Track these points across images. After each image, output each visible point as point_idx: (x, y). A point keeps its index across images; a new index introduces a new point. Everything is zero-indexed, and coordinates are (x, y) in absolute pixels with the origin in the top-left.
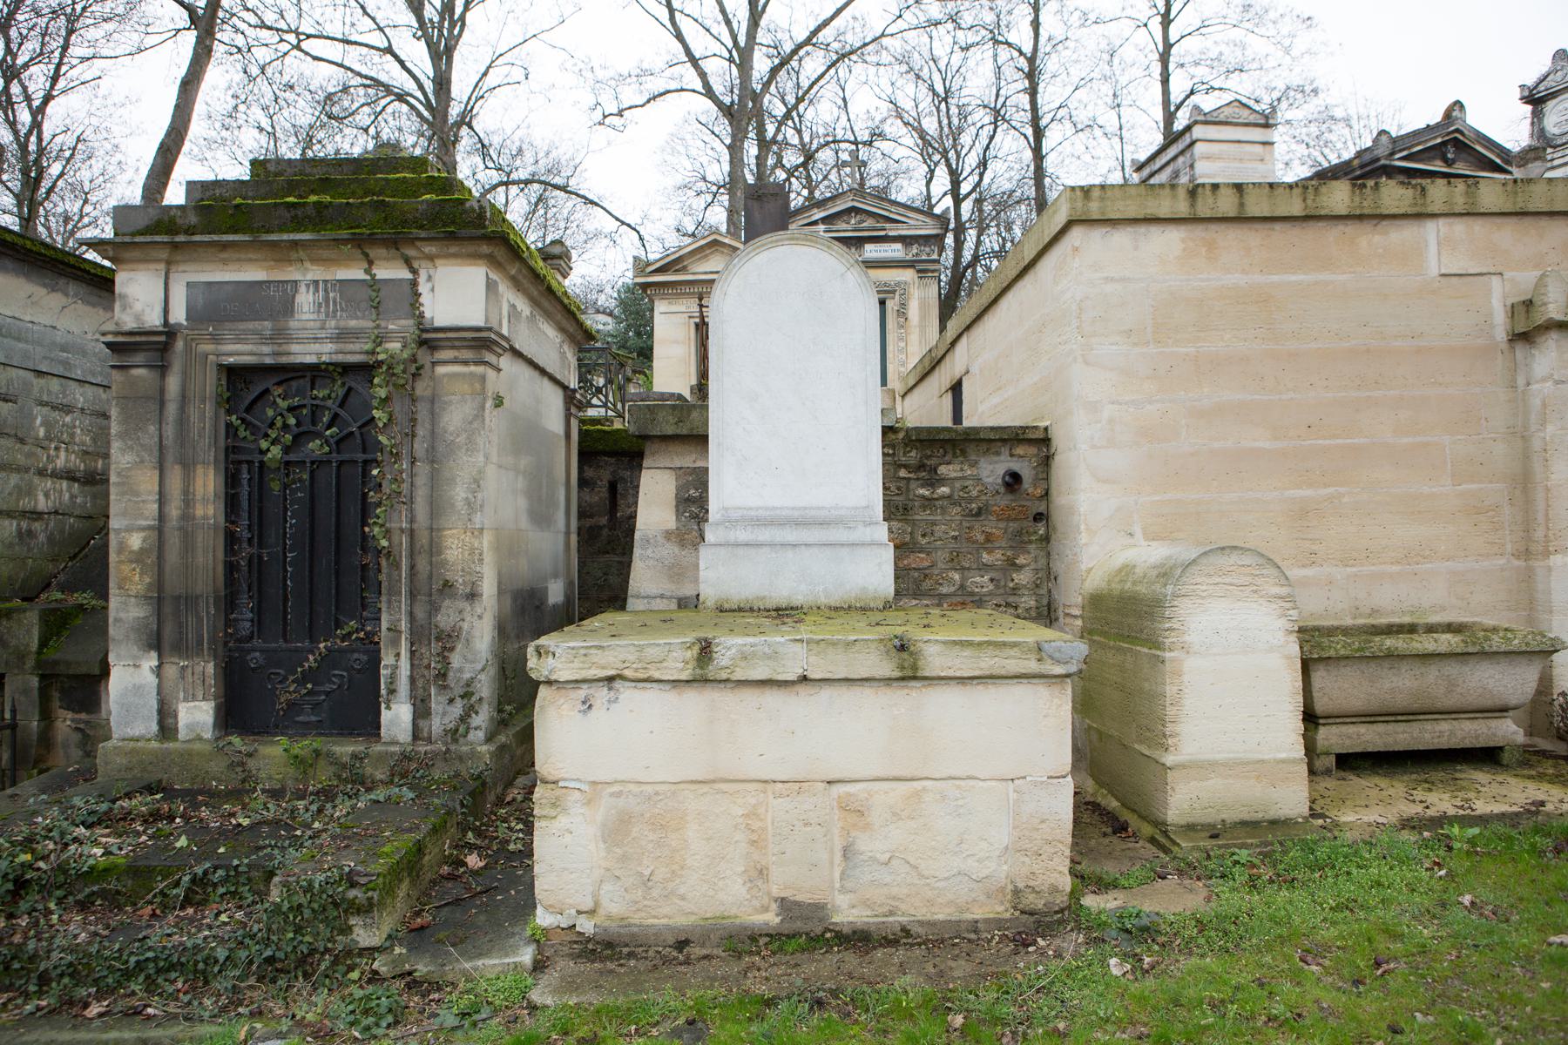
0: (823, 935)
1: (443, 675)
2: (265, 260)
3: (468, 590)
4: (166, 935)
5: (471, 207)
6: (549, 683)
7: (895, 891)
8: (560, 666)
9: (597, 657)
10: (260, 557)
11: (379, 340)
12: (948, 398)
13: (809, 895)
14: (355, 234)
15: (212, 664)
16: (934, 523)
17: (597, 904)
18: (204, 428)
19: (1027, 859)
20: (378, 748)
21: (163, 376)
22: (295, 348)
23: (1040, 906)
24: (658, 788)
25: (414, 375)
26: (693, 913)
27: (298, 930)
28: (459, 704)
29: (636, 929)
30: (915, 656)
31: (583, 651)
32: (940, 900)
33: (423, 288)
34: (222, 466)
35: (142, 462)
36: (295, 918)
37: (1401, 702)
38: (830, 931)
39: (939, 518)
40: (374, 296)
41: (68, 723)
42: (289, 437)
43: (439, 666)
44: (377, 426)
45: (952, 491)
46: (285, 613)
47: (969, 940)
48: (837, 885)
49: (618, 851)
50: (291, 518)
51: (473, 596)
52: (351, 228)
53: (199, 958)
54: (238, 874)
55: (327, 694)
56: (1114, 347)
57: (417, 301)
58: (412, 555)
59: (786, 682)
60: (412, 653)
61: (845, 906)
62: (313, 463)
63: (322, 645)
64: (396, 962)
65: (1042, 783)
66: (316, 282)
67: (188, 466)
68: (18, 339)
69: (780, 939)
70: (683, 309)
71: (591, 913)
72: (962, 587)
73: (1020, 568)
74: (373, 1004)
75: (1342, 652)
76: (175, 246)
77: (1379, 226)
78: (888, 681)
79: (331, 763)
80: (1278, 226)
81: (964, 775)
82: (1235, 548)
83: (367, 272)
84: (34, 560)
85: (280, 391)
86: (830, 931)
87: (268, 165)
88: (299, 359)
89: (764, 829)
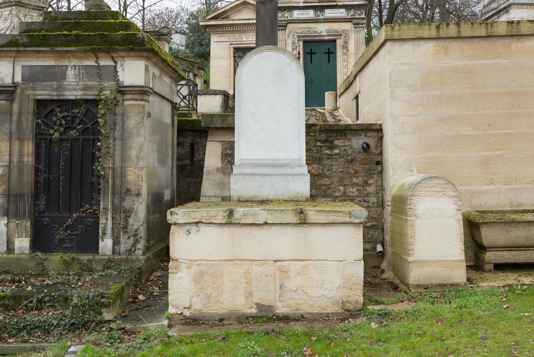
0: (272, 317)
1: (125, 227)
2: (54, 57)
3: (136, 192)
4: (32, 317)
5: (139, 37)
6: (175, 224)
7: (299, 302)
8: (179, 218)
9: (193, 215)
10: (49, 178)
11: (101, 91)
12: (355, 101)
13: (267, 302)
14: (92, 48)
15: (29, 222)
16: (332, 165)
17: (191, 305)
18: (28, 125)
20: (98, 257)
21: (12, 104)
22: (66, 93)
23: (352, 308)
24: (214, 262)
25: (115, 105)
26: (226, 309)
27: (84, 313)
29: (205, 314)
30: (305, 215)
31: (188, 213)
32: (315, 305)
33: (119, 69)
34: (34, 140)
35: (3, 139)
36: (83, 308)
37: (521, 242)
38: (275, 316)
39: (334, 163)
42: (62, 129)
43: (124, 223)
44: (99, 125)
47: (325, 320)
48: (278, 299)
49: (199, 285)
50: (62, 162)
51: (138, 195)
53: (46, 324)
55: (76, 235)
56: (404, 92)
57: (116, 74)
58: (114, 178)
60: (113, 218)
61: (280, 307)
62: (72, 139)
64: (118, 325)
65: (352, 262)
66: (75, 66)
67: (21, 141)
69: (257, 319)
70: (227, 39)
71: (189, 308)
72: (344, 193)
73: (370, 185)
75: (492, 220)
76: (18, 51)
77: (521, 39)
78: (296, 224)
80: (476, 40)
81: (323, 259)
82: (436, 177)
83: (96, 62)
86: (275, 316)
87: (51, 14)
88: (68, 98)
89: (252, 278)
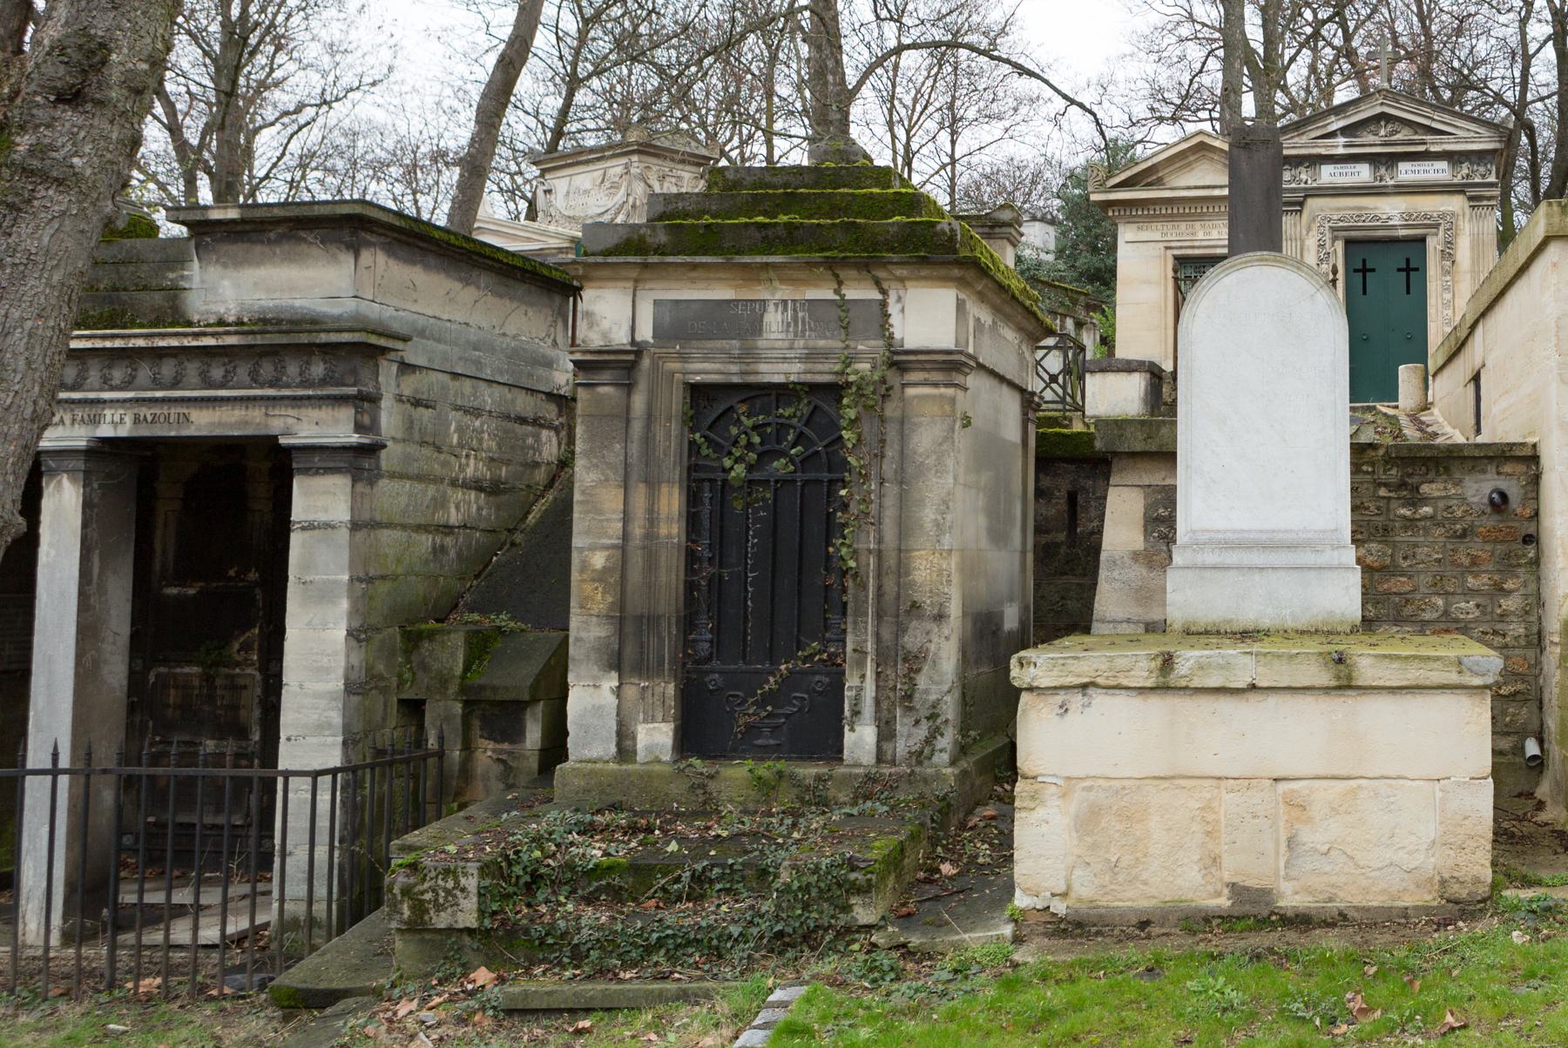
0: (1269, 917)
1: (909, 697)
3: (935, 612)
6: (1031, 689)
7: (1333, 879)
9: (1075, 666)
10: (721, 577)
12: (1472, 386)
13: (1257, 881)
14: (827, 257)
16: (1416, 545)
17: (1069, 887)
19: (1452, 852)
20: (841, 770)
21: (629, 394)
22: (763, 367)
25: (883, 396)
27: (806, 907)
28: (925, 725)
31: (1061, 661)
33: (893, 309)
34: (685, 485)
35: (607, 480)
38: (1276, 914)
39: (1422, 539)
40: (843, 316)
41: (489, 753)
42: (753, 456)
43: (906, 687)
45: (1435, 511)
46: (745, 634)
48: (1282, 873)
49: (1089, 839)
50: (753, 538)
51: (940, 617)
52: (822, 250)
54: (733, 871)
55: (787, 716)
57: (887, 322)
59: (1238, 689)
60: (878, 674)
61: (1289, 892)
62: (777, 482)
63: (783, 667)
64: (890, 936)
66: (785, 302)
67: (652, 484)
68: (439, 341)
70: (1157, 236)
71: (1065, 895)
72: (1446, 613)
73: (1508, 593)
74: (878, 964)
76: (646, 266)
78: (1326, 690)
79: (794, 786)
83: (837, 292)
84: (445, 578)
85: (744, 409)
86: (1276, 914)
87: (726, 173)
88: (767, 379)
89: (1217, 821)
